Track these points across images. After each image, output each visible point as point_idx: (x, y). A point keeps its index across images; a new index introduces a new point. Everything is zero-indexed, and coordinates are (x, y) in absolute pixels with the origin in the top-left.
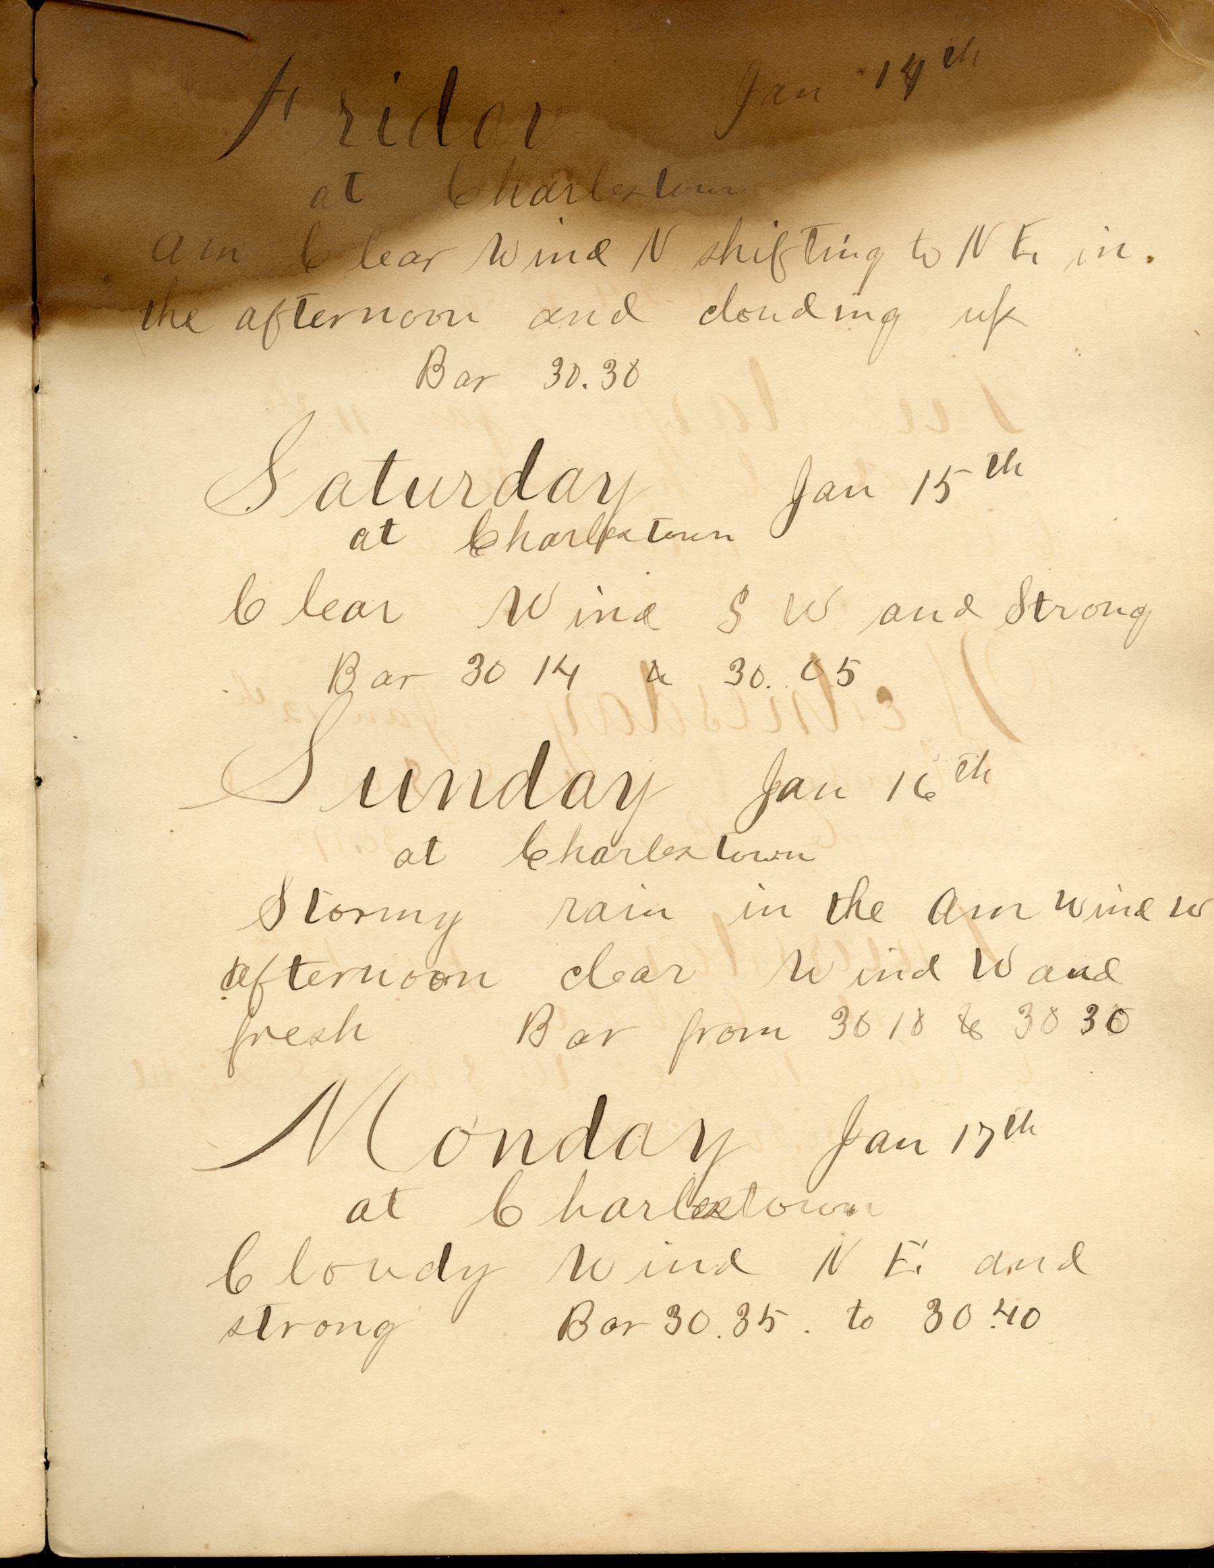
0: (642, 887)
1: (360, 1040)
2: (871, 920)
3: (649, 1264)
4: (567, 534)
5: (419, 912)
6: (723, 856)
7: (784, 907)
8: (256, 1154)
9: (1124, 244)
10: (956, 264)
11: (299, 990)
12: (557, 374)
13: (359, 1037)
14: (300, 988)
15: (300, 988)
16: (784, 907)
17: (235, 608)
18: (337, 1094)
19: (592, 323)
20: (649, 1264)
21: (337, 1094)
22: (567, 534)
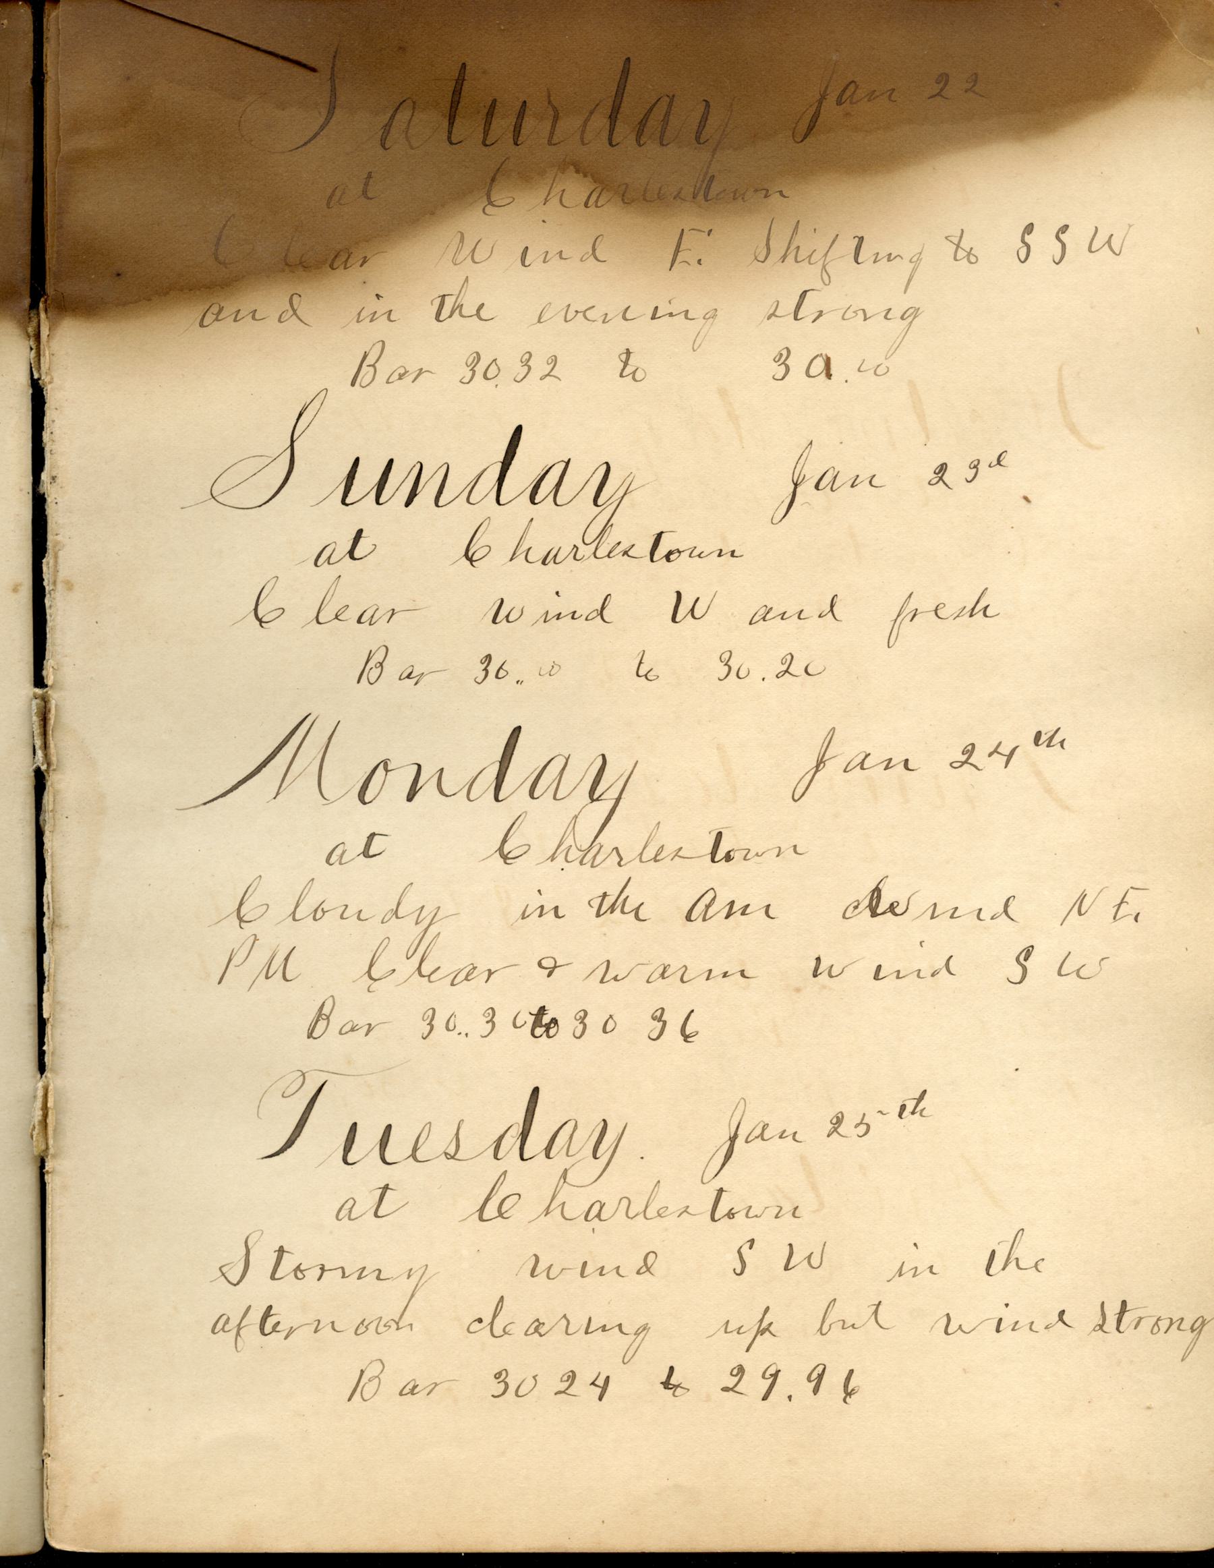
0: (592, 1230)
1: (473, 801)
2: (499, 1218)
3: (278, 794)
4: (757, 622)
5: (980, 910)
6: (525, 1158)
7: (618, 1268)
8: (249, 955)
9: (728, 1321)
10: (218, 981)
11: (529, 1160)
12: (486, 669)
13: (288, 977)
14: (530, 1158)
15: (530, 1158)
16: (618, 1268)
17: (417, 966)
18: (615, 510)
19: (530, 560)
20: (278, 794)
21: (615, 510)
22: (757, 622)
